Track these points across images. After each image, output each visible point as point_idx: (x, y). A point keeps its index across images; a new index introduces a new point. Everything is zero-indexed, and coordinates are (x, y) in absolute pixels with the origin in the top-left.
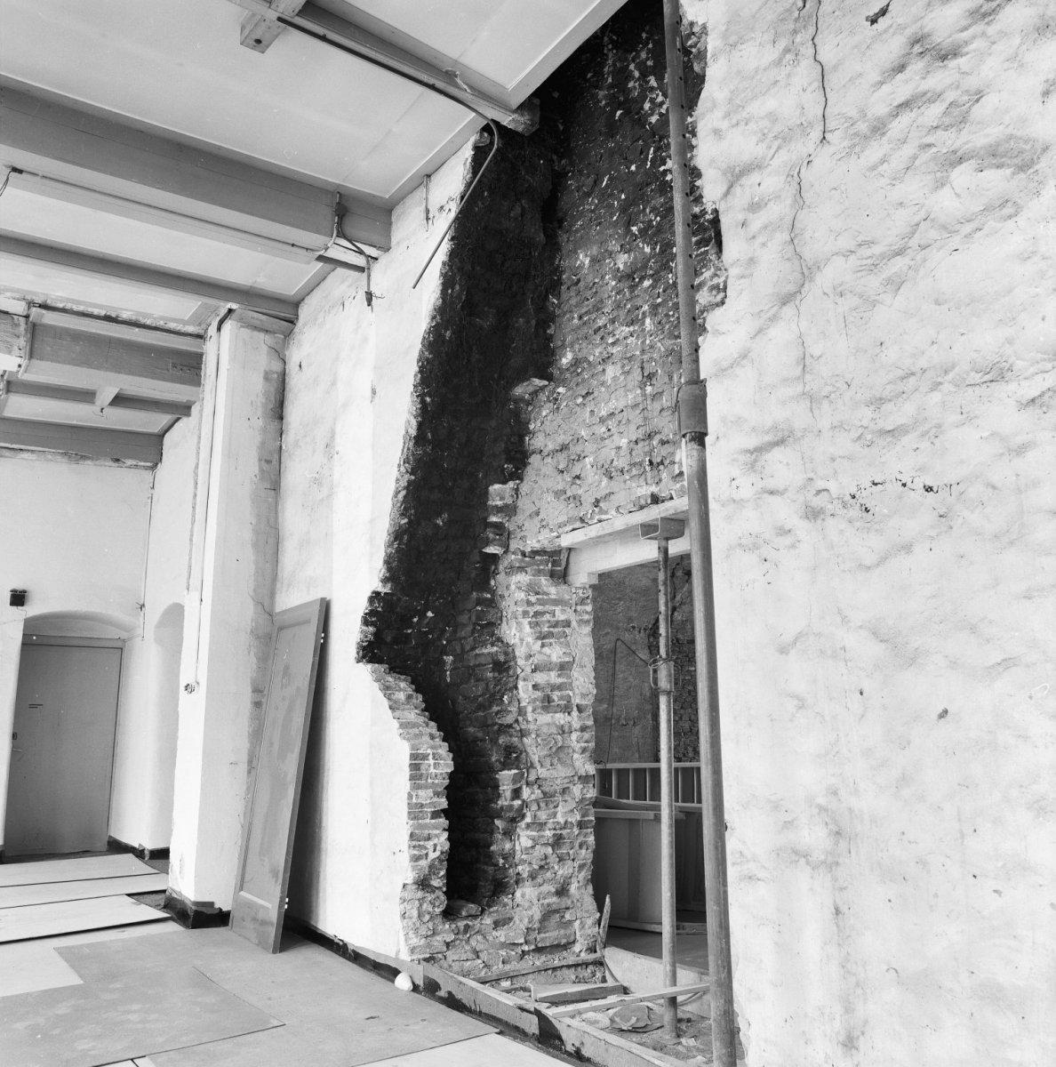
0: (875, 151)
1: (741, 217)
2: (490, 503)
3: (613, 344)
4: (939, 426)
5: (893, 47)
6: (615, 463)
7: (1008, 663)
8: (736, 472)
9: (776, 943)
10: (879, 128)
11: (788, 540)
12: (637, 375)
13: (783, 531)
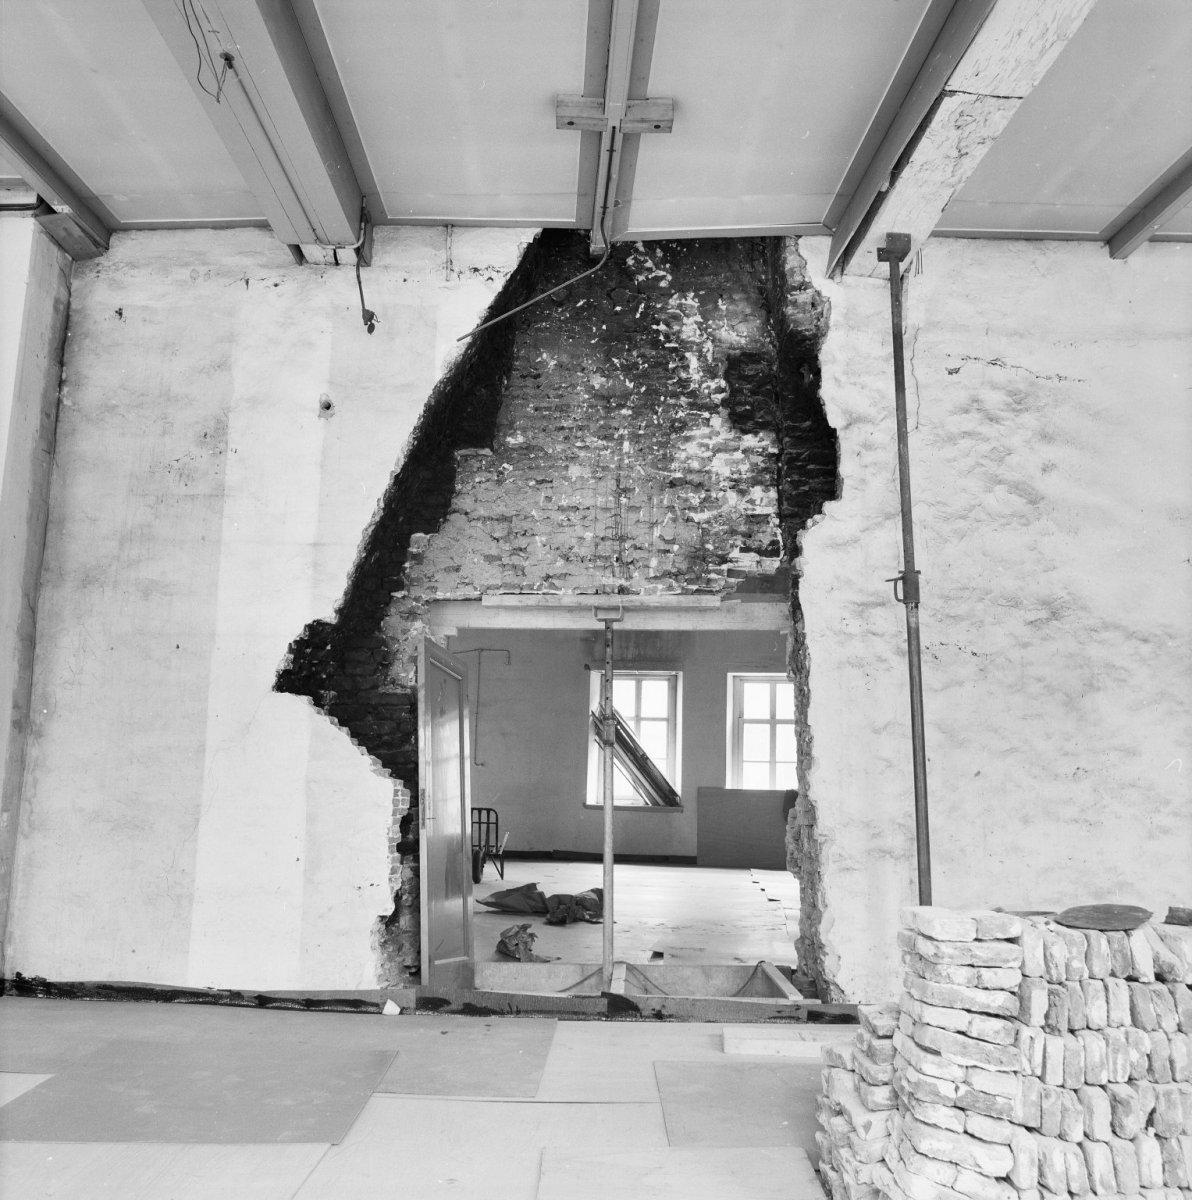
0: (949, 451)
1: (857, 449)
2: (410, 549)
3: (580, 448)
4: (982, 622)
5: (962, 397)
6: (575, 550)
7: (1013, 750)
8: (846, 615)
9: (866, 906)
10: (951, 439)
11: (884, 666)
12: (611, 484)
13: (881, 659)
